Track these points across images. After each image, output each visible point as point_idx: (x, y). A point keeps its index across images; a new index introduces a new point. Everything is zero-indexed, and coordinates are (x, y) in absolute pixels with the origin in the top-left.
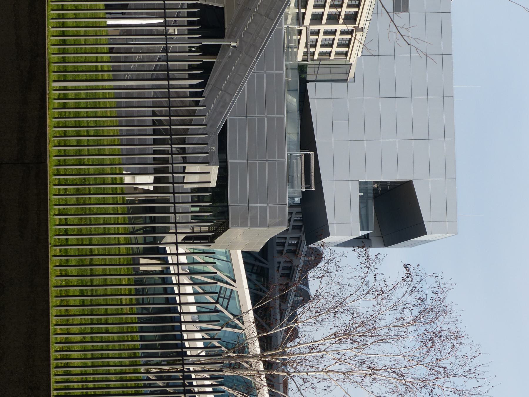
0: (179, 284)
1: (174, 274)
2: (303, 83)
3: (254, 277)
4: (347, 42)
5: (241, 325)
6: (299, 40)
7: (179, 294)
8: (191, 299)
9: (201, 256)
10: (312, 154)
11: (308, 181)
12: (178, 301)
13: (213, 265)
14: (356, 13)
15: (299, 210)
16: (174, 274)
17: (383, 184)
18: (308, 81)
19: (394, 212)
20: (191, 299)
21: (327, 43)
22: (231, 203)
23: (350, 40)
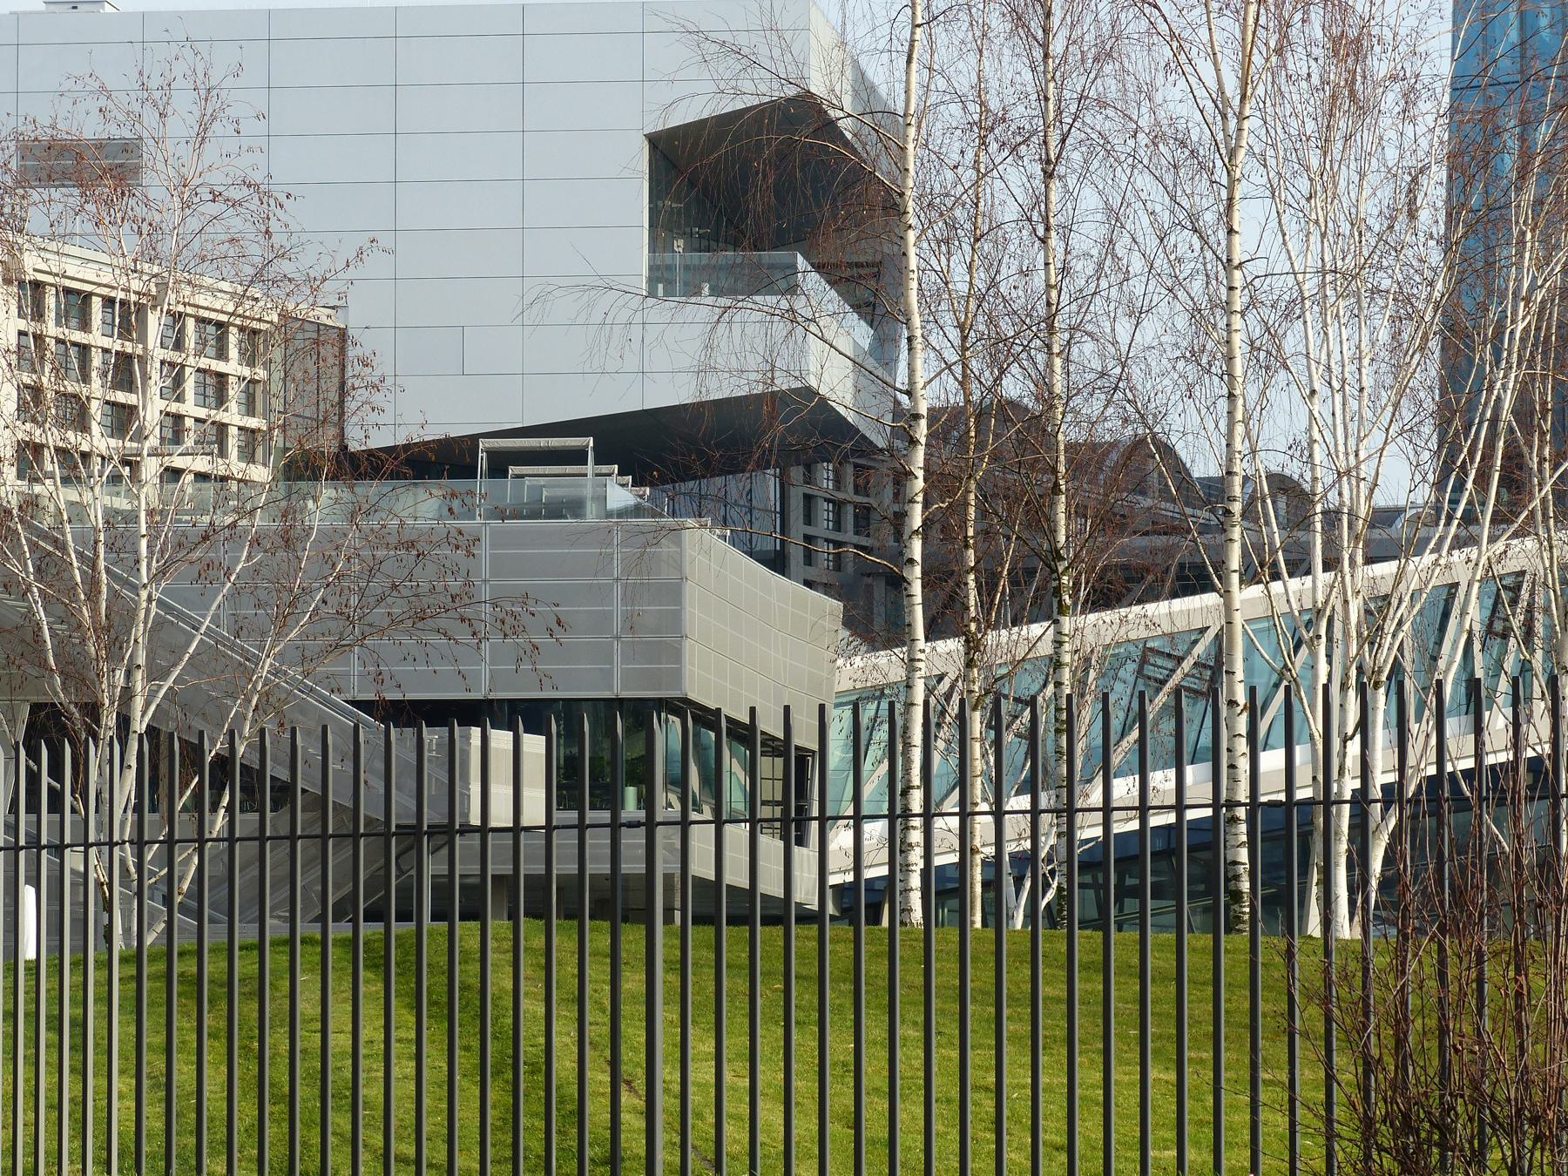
0: (1143, 809)
1: (1143, 821)
2: (359, 466)
3: (1139, 590)
4: (211, 329)
5: (1210, 635)
6: (201, 477)
7: (1180, 807)
8: (1162, 781)
9: (867, 767)
10: (483, 444)
11: (578, 457)
12: (1171, 818)
13: (933, 729)
14: (109, 302)
15: (796, 473)
16: (1143, 821)
17: (662, 225)
18: (344, 447)
19: (760, 188)
20: (1162, 781)
21: (210, 391)
22: (611, 689)
23: (201, 321)
